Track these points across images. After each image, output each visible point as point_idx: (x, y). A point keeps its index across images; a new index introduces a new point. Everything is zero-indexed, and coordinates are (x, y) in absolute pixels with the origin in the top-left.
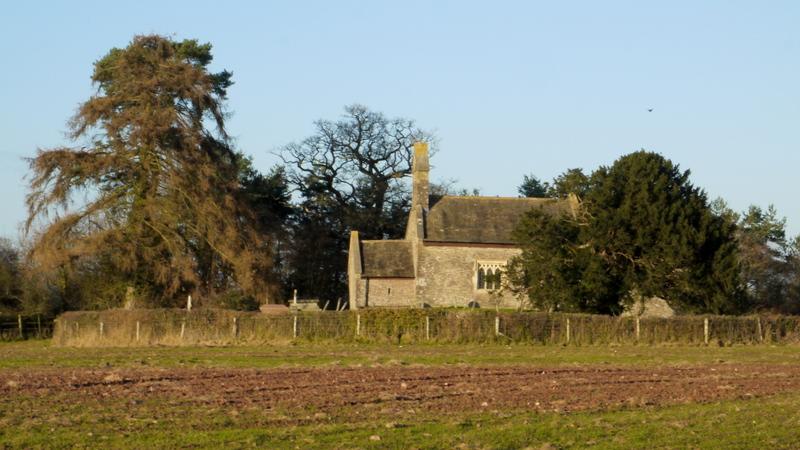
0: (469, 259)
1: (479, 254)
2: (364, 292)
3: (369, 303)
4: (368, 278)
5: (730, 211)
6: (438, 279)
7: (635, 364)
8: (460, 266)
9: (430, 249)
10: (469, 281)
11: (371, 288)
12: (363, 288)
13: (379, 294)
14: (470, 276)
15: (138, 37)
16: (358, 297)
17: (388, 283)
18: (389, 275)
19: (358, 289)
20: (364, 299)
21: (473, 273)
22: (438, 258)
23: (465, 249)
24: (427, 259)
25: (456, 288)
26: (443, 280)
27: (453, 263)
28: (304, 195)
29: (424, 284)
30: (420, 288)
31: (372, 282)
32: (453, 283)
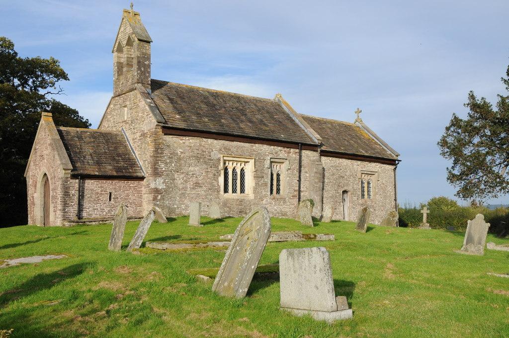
0: (215, 155)
1: (225, 148)
2: (76, 198)
3: (84, 214)
4: (84, 177)
5: (16, 53)
6: (179, 179)
7: (495, 292)
8: (205, 163)
9: (169, 139)
10: (215, 183)
11: (87, 193)
12: (74, 192)
13: (97, 200)
14: (216, 177)
15: (444, 143)
16: (65, 204)
17: (109, 185)
18: (109, 173)
19: (66, 193)
20: (76, 207)
21: (218, 172)
22: (179, 151)
23: (210, 141)
24: (166, 152)
25: (202, 191)
26: (186, 181)
27: (198, 158)
28: (38, 90)
29: (161, 186)
30: (157, 191)
31: (90, 184)
32: (197, 185)
